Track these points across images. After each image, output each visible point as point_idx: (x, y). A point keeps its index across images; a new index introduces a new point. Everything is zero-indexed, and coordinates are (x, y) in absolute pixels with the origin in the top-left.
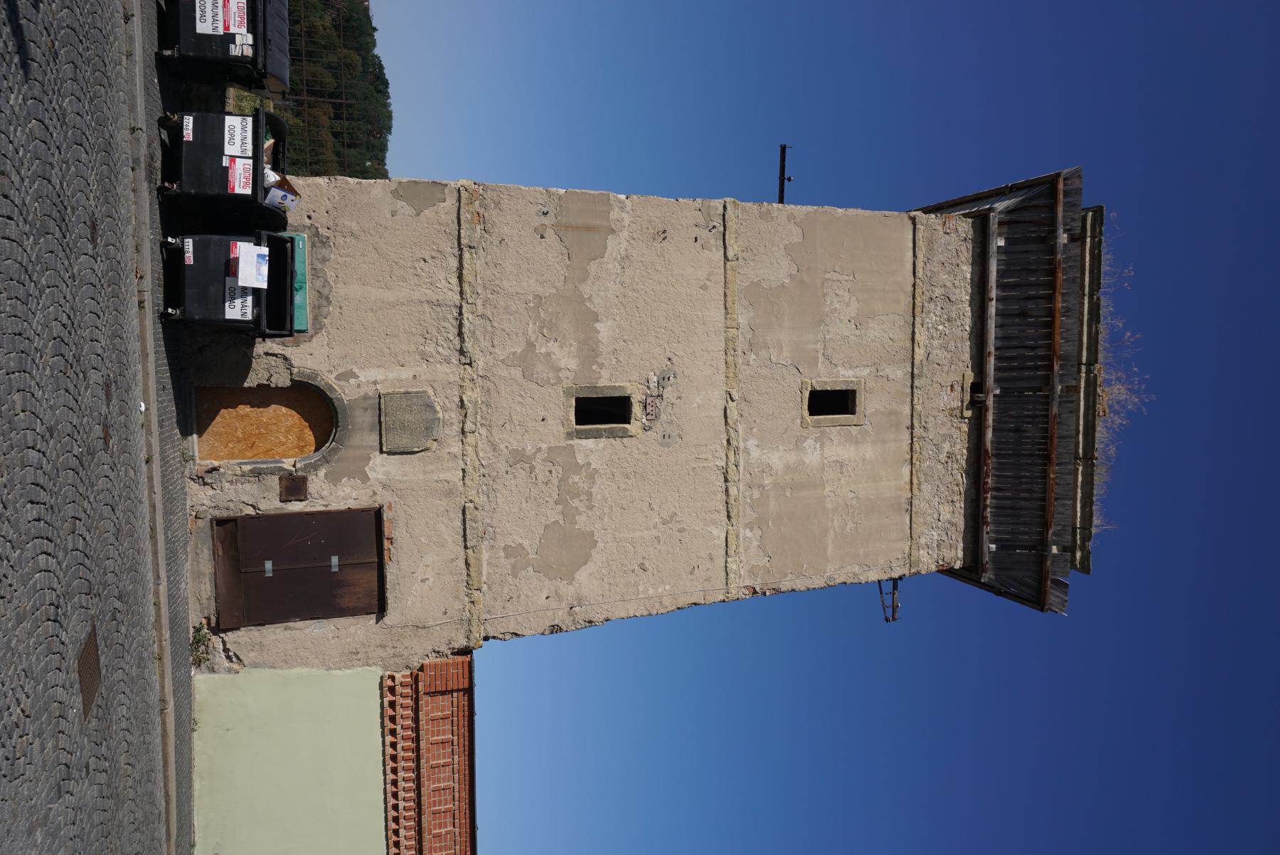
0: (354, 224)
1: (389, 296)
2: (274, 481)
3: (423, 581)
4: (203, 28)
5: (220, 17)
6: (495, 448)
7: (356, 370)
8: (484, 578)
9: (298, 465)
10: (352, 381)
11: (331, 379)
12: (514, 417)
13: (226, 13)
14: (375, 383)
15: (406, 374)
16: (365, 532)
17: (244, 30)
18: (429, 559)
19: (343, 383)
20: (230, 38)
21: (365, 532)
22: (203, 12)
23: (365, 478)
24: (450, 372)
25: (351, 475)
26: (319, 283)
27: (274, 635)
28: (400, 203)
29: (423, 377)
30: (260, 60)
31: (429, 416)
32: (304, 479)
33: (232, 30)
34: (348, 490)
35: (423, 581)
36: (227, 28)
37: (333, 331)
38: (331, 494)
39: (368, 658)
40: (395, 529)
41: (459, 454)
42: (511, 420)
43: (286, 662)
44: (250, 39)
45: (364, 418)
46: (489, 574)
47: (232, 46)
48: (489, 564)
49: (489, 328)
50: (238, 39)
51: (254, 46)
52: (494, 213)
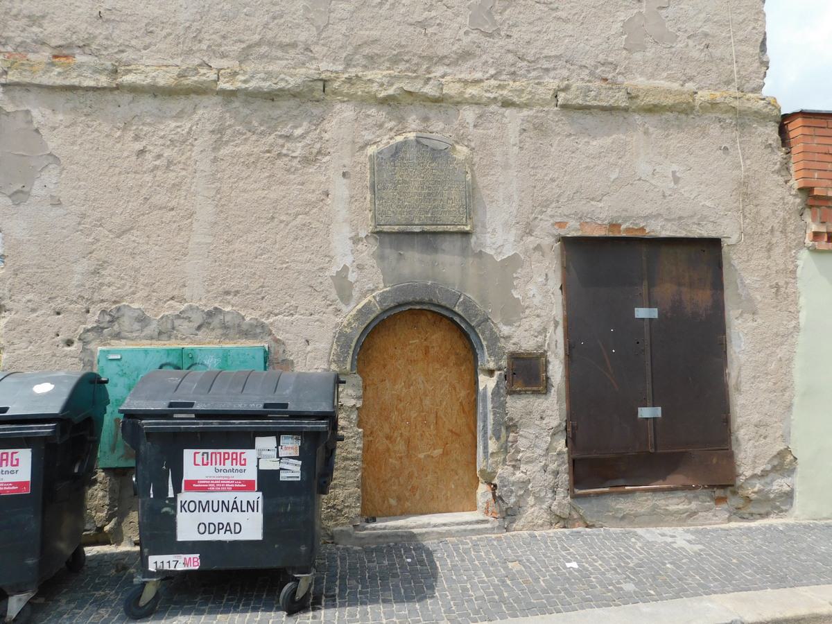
0: (78, 268)
1: (205, 212)
2: (516, 405)
3: (676, 180)
4: (251, 527)
5: (229, 497)
6: (465, 55)
7: (334, 270)
8: (675, 86)
9: (492, 365)
10: (352, 277)
11: (350, 311)
12: (417, 17)
13: (220, 487)
14: (356, 240)
15: (341, 189)
16: (603, 264)
17: (250, 455)
18: (643, 168)
19: (356, 294)
20: (268, 481)
21: (603, 264)
22: (220, 527)
23: (513, 262)
24: (341, 121)
25: (507, 285)
26: (184, 326)
27: (748, 406)
28: (37, 189)
29: (346, 161)
30: (308, 425)
31: (412, 154)
32: (515, 358)
33: (252, 475)
34: (532, 289)
35: (676, 180)
36: (248, 486)
37: (266, 306)
38: (534, 312)
39: (785, 270)
40: (599, 216)
41: (478, 110)
42: (423, 24)
43: (784, 390)
44: (265, 443)
45: (414, 264)
46: (668, 78)
47: (284, 476)
48: (652, 76)
49: (264, 49)
50: (269, 464)
51: (277, 434)
52: (49, 27)
